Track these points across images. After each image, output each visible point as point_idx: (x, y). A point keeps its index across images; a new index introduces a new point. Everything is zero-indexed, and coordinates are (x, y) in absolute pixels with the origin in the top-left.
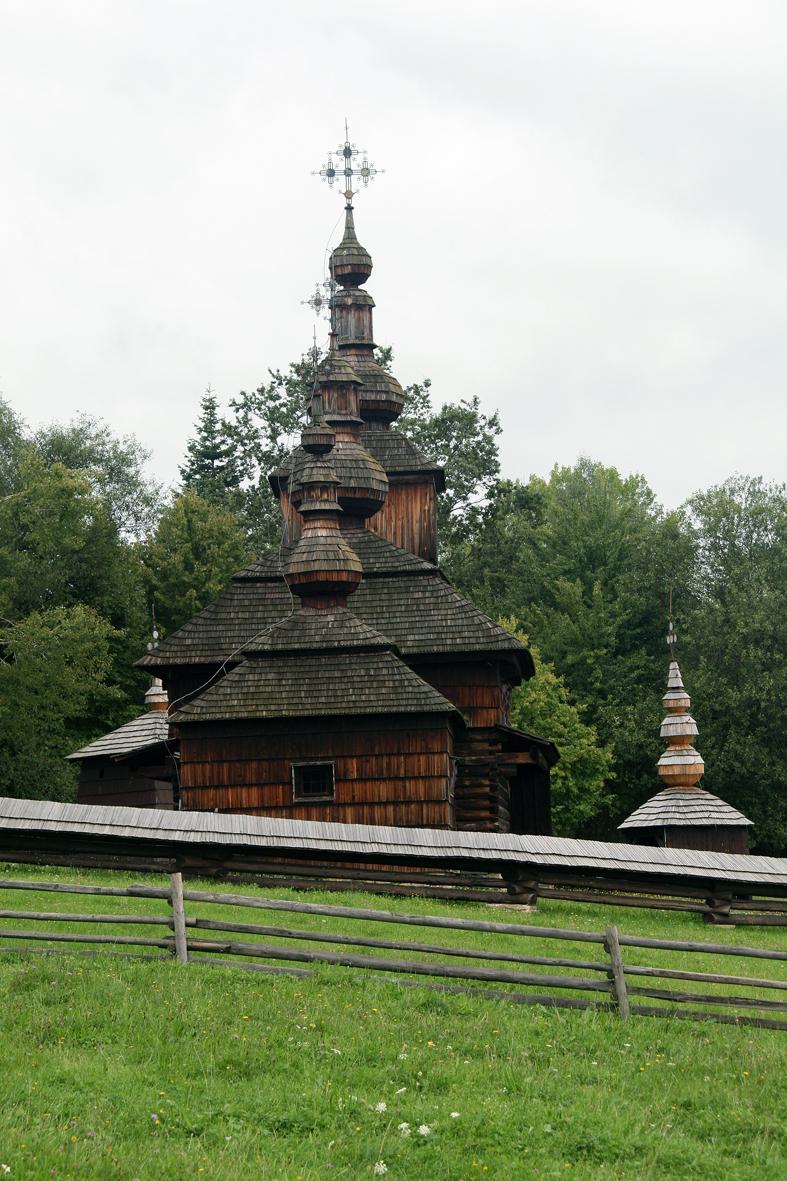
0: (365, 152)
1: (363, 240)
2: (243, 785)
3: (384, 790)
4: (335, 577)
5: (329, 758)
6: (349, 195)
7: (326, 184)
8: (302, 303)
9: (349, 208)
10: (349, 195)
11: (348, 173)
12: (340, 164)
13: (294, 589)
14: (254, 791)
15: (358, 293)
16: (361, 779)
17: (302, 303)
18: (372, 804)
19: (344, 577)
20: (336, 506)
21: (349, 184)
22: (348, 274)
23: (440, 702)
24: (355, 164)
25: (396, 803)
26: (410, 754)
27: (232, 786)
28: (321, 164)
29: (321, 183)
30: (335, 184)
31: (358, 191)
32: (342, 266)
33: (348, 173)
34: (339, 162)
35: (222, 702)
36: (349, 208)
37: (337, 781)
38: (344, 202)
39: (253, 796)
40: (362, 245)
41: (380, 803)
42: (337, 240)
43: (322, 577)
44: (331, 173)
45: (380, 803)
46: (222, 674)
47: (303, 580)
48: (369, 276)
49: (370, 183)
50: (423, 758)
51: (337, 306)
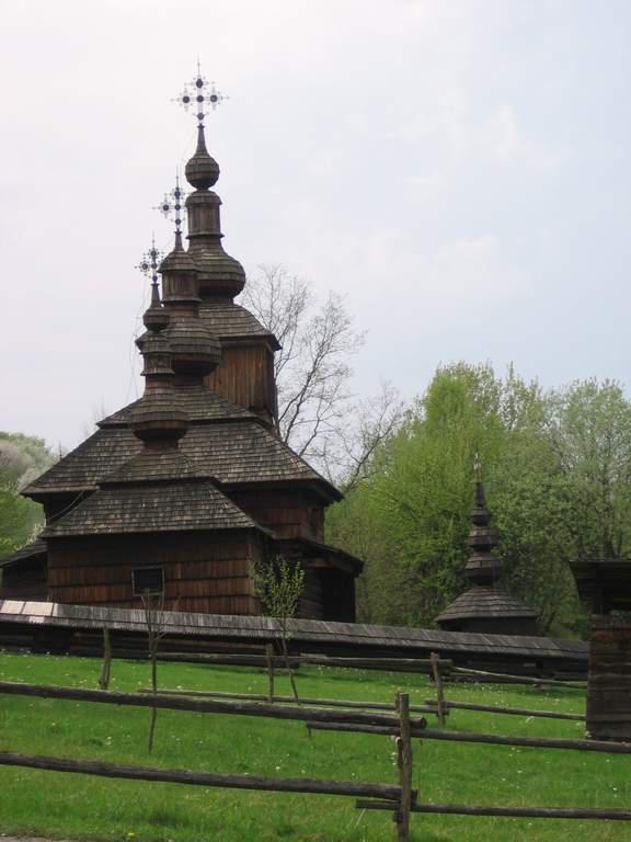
0: (213, 83)
1: (212, 152)
2: (95, 585)
3: (201, 587)
4: (168, 426)
5: (160, 564)
6: (201, 117)
7: (163, 215)
8: (154, 208)
9: (201, 127)
10: (201, 117)
11: (200, 99)
12: (194, 93)
13: (137, 434)
14: (104, 589)
15: (207, 194)
16: (185, 579)
17: (154, 208)
18: (192, 598)
19: (175, 425)
20: (170, 371)
21: (178, 215)
22: (37, 626)
23: (244, 520)
24: (206, 92)
25: (210, 597)
26: (221, 560)
27: (88, 585)
28: (160, 202)
29: (159, 213)
30: (190, 107)
31: (208, 113)
32: (194, 173)
33: (200, 99)
34: (193, 91)
35: (87, 523)
36: (201, 127)
37: (166, 580)
38: (197, 122)
39: (103, 592)
40: (212, 156)
41: (198, 597)
42: (192, 151)
43: (158, 425)
44: (166, 208)
45: (198, 597)
46: (80, 500)
47: (144, 428)
48: (218, 172)
49: (218, 106)
50: (230, 563)
51: (192, 205)
